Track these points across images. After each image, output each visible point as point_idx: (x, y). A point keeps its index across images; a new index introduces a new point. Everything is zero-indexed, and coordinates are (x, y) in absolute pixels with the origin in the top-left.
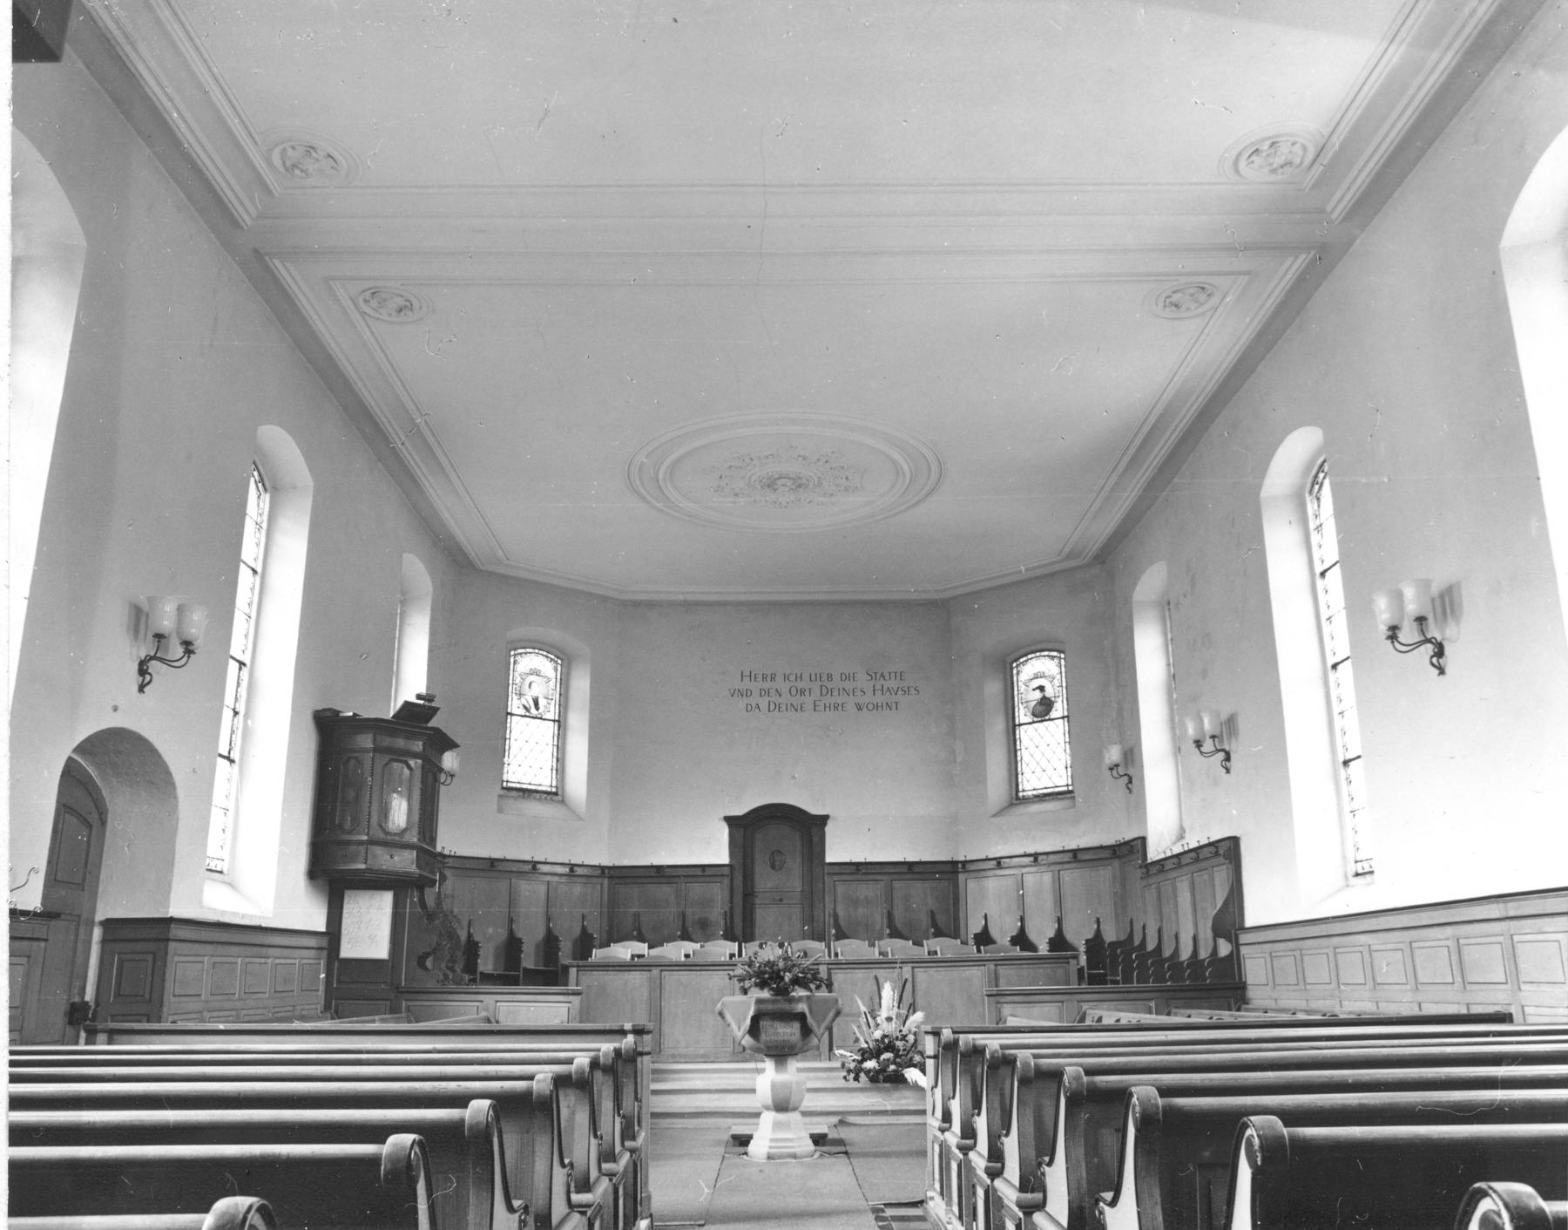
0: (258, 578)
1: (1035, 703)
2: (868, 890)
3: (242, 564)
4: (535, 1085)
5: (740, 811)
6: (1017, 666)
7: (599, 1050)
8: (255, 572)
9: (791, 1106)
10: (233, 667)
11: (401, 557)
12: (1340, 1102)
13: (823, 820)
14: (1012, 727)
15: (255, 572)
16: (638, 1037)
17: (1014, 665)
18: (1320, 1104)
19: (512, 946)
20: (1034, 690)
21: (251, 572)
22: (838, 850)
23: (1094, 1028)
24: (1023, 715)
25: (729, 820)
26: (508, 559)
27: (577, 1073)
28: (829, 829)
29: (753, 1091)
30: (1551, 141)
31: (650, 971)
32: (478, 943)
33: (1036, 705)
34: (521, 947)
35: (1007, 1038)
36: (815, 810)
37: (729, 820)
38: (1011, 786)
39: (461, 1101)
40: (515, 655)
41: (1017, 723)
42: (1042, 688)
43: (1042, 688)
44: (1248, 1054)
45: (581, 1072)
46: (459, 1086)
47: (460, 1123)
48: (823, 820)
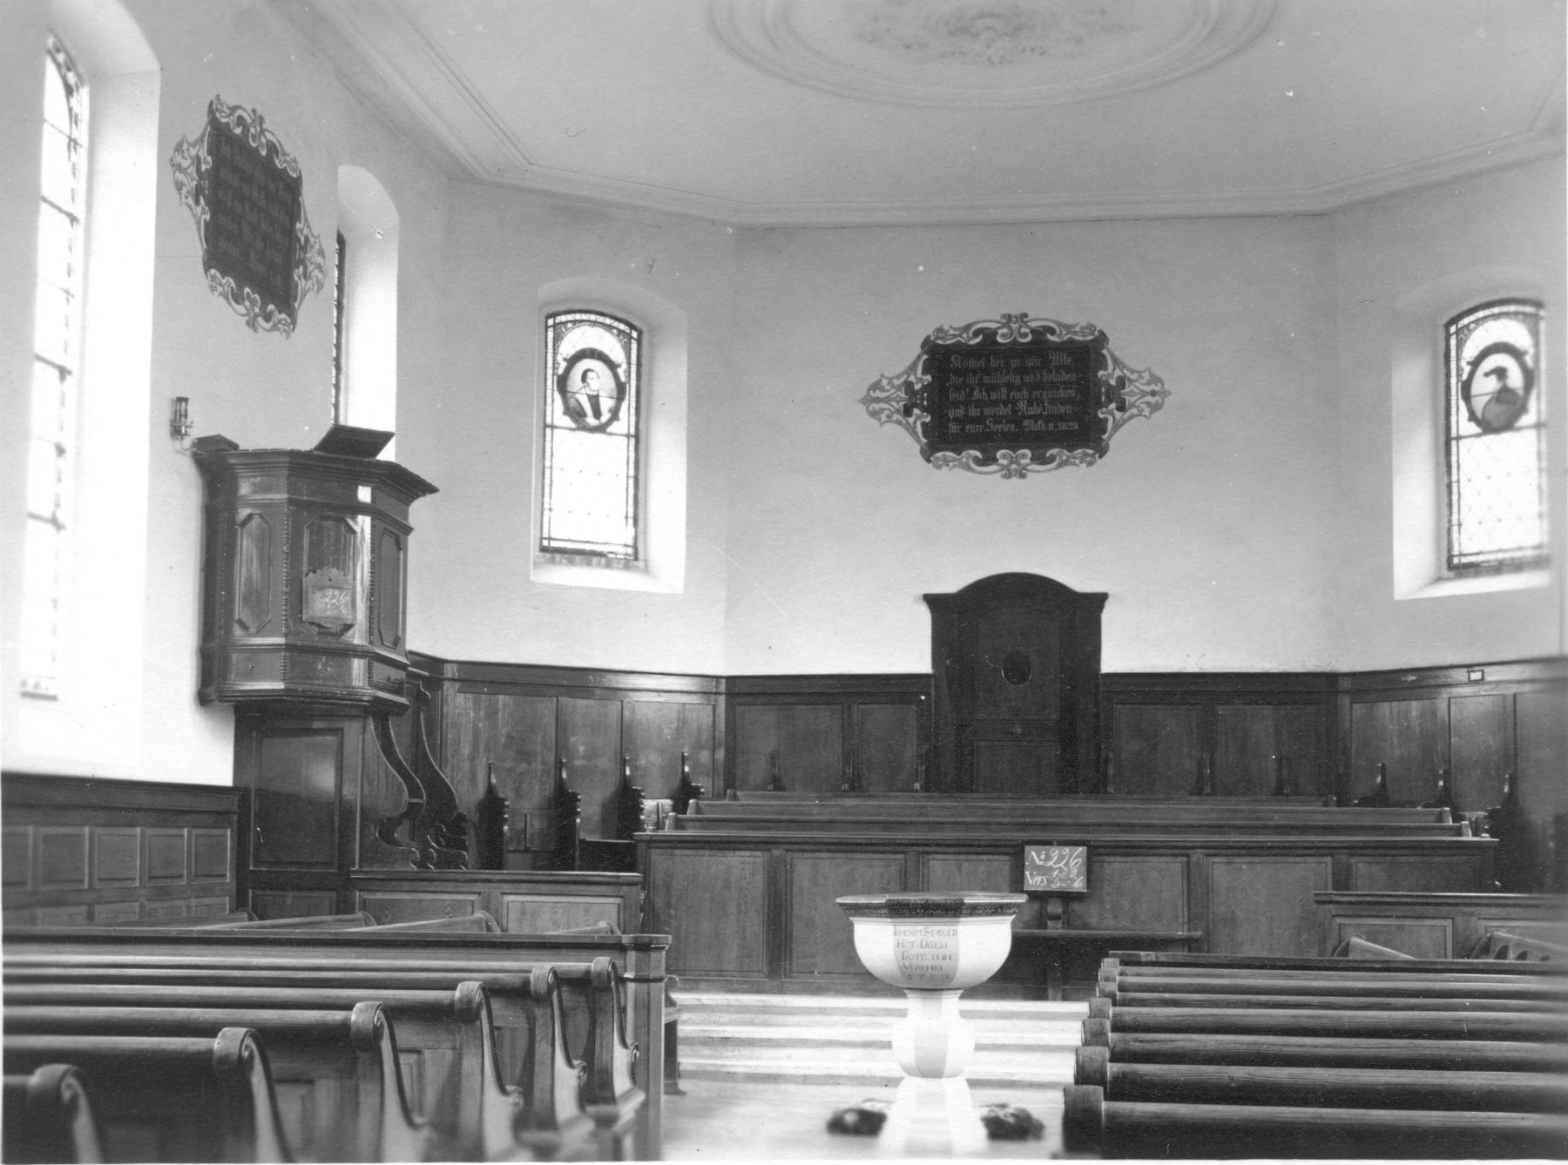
0: (80, 229)
1: (1487, 398)
2: (1172, 722)
3: (44, 207)
4: (353, 1016)
5: (951, 585)
6: (1457, 333)
7: (529, 971)
8: (73, 219)
9: (948, 1068)
10: (43, 377)
11: (335, 174)
12: (135, 1046)
13: (1098, 600)
14: (1447, 441)
15: (73, 219)
16: (641, 955)
17: (1453, 329)
18: (164, 1046)
19: (563, 802)
20: (1487, 375)
21: (67, 220)
22: (1117, 657)
23: (1537, 969)
24: (1463, 424)
25: (933, 601)
26: (531, 164)
27: (461, 1000)
28: (1107, 616)
29: (887, 1045)
30: (155, 292)
31: (769, 850)
32: (503, 800)
33: (1490, 401)
34: (575, 808)
35: (1422, 980)
36: (1080, 582)
37: (933, 601)
38: (1438, 551)
39: (211, 1030)
40: (555, 325)
41: (1454, 433)
42: (1501, 373)
43: (1501, 373)
44: (1424, 1014)
45: (467, 1002)
46: (78, 1012)
47: (206, 1056)
48: (1098, 600)
